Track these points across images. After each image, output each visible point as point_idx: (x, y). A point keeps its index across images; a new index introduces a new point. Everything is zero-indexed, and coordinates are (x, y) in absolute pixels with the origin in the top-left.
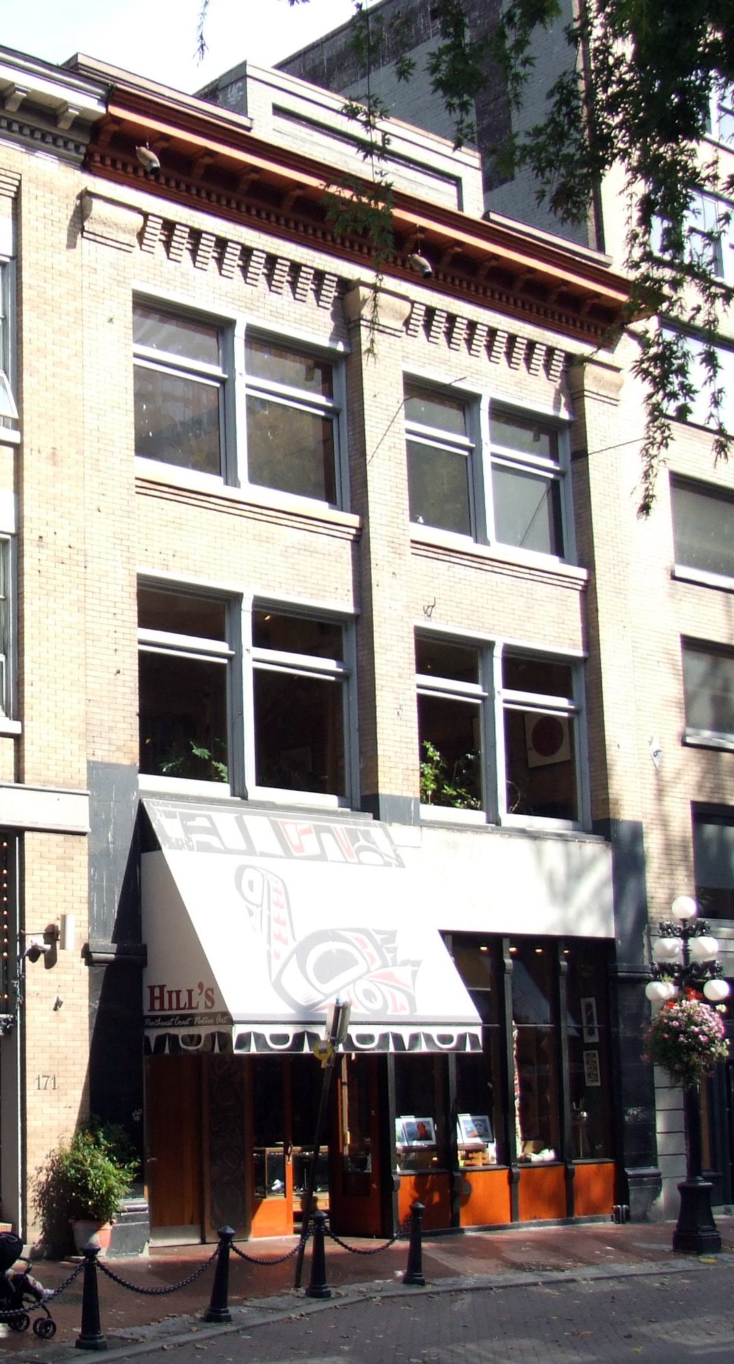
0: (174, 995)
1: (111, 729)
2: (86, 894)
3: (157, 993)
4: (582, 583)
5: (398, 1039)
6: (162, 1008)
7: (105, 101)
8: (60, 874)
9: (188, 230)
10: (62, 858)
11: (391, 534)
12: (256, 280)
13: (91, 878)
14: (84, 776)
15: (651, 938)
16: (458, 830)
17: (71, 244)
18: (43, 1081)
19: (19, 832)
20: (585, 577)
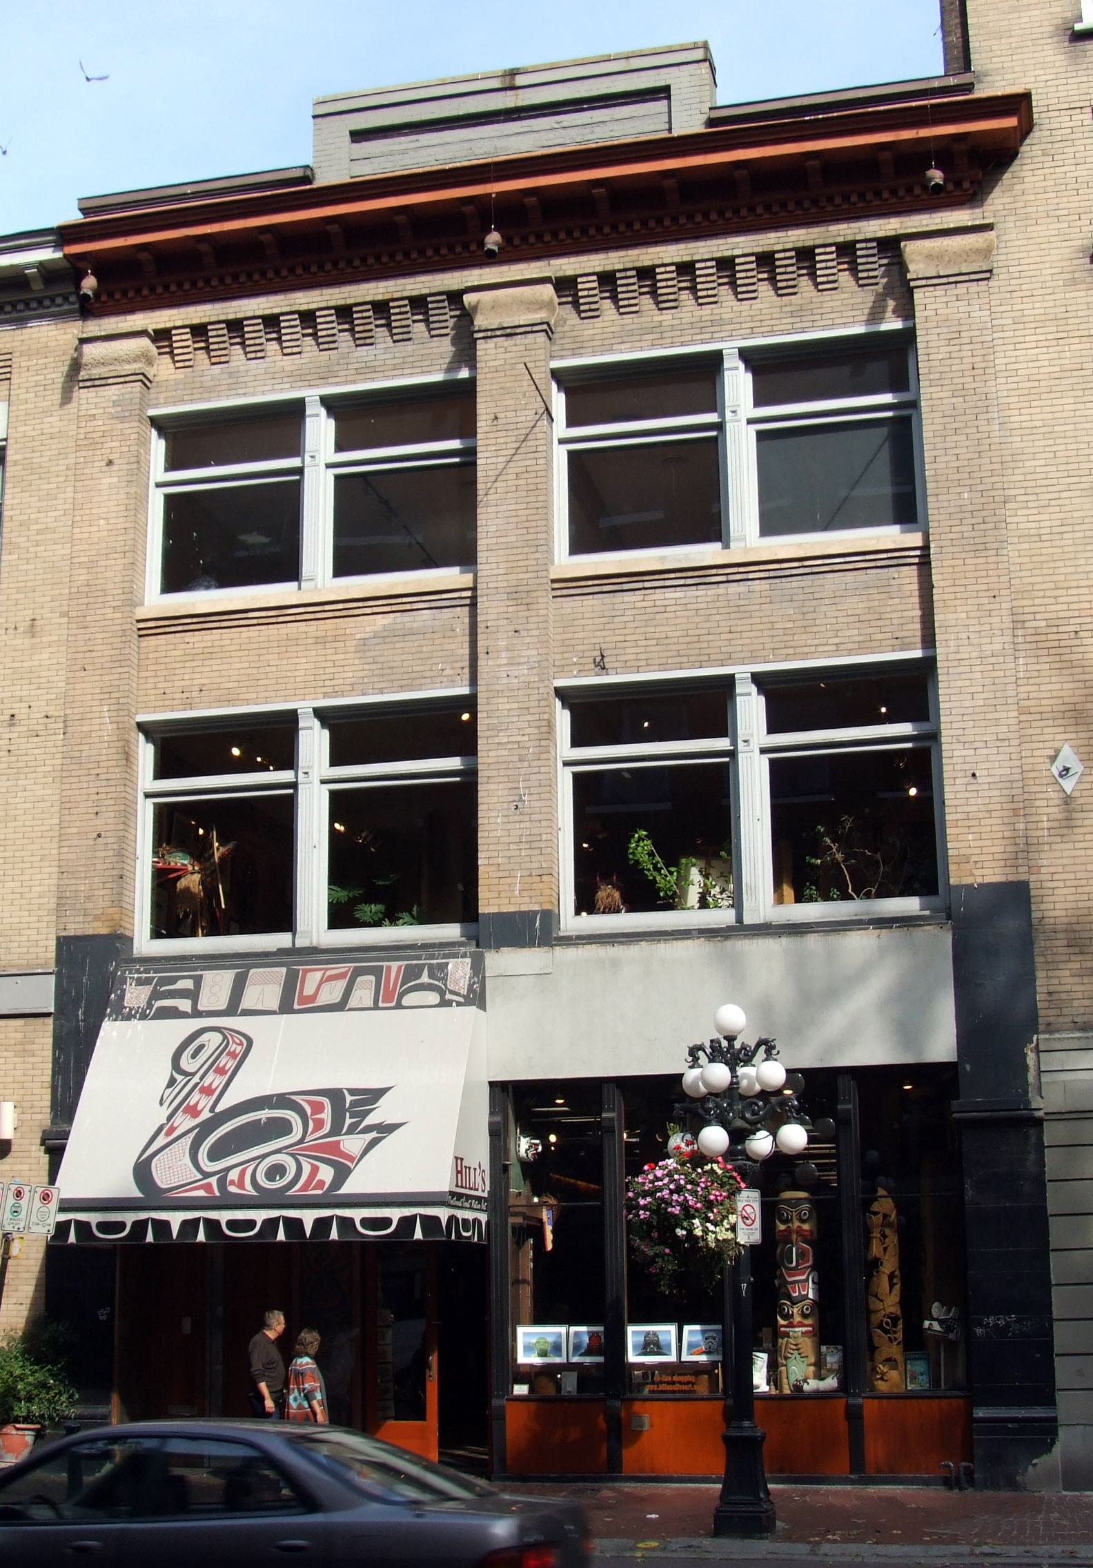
1: (88, 898)
2: (49, 1079)
4: (918, 553)
5: (294, 1226)
7: (58, 245)
8: (17, 1060)
9: (260, 321)
10: (21, 1044)
11: (514, 583)
12: (334, 342)
13: (55, 1061)
14: (52, 954)
15: (1041, 1054)
16: (621, 943)
17: (66, 398)
20: (919, 543)
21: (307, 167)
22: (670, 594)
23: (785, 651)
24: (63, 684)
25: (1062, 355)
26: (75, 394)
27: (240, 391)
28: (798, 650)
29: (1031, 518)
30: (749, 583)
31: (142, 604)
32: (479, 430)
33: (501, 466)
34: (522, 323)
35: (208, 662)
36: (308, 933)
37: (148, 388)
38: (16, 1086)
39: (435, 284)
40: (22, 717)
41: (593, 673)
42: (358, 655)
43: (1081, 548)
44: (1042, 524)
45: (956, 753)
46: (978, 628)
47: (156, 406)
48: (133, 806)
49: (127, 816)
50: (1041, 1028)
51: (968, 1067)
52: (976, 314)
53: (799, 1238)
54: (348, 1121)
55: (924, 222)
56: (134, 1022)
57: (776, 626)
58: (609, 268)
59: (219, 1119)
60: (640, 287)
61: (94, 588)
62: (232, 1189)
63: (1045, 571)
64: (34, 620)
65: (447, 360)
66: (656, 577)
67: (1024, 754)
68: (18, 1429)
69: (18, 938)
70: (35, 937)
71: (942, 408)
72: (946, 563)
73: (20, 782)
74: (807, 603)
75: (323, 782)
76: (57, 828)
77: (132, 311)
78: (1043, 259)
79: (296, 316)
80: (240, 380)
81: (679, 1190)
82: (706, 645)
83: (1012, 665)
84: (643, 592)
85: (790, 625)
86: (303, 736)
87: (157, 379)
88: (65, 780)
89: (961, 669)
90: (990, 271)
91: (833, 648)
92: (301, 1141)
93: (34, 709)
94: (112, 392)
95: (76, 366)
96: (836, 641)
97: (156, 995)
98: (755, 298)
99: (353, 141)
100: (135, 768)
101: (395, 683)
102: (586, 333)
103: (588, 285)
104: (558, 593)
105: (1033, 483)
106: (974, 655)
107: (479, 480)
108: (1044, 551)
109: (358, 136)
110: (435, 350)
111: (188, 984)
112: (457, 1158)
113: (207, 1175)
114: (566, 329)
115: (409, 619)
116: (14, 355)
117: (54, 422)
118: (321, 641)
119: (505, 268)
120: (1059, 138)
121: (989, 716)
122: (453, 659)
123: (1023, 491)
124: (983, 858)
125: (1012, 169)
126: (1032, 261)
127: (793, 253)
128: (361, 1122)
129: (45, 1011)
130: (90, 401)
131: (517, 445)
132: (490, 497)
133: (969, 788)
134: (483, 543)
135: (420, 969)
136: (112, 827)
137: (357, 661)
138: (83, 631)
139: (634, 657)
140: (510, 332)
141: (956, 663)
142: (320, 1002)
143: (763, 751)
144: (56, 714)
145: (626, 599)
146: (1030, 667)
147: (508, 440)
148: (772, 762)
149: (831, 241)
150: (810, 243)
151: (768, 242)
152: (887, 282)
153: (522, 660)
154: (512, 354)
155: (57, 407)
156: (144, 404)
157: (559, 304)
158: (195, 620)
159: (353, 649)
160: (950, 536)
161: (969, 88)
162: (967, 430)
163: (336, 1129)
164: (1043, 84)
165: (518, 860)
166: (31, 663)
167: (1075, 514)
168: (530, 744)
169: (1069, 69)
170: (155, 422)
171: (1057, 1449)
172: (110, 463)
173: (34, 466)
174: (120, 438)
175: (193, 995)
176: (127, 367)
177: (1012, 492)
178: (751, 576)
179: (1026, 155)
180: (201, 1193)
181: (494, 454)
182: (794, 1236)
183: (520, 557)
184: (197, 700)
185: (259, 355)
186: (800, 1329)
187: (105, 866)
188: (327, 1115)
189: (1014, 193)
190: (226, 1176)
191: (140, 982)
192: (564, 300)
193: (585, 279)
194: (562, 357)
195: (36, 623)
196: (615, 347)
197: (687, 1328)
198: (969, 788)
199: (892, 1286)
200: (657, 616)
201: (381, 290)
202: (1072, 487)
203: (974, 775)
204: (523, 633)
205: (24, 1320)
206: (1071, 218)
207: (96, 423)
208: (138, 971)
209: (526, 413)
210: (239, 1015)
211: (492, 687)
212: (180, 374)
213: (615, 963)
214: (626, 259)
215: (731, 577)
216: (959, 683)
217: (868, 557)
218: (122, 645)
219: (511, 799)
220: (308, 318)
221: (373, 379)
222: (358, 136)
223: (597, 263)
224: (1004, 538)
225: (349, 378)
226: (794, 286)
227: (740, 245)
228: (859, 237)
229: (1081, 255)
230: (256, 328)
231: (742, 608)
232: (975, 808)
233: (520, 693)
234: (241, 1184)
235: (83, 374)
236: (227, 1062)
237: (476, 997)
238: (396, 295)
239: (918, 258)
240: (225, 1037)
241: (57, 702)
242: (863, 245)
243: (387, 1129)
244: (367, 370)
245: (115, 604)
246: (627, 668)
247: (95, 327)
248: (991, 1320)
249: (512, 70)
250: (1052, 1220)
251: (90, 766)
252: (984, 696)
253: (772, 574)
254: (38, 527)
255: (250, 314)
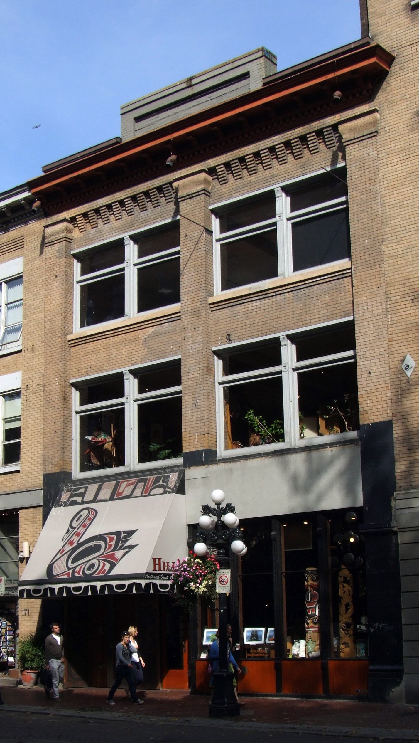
0: (166, 564)
1: (52, 457)
3: (157, 562)
5: (94, 588)
6: (160, 570)
11: (194, 307)
12: (133, 211)
16: (234, 461)
17: (41, 252)
18: (24, 612)
19: (17, 510)
21: (118, 137)
22: (255, 304)
23: (298, 324)
24: (43, 371)
25: (407, 166)
26: (44, 250)
27: (102, 238)
28: (304, 322)
29: (394, 248)
30: (285, 294)
31: (72, 333)
32: (181, 242)
33: (188, 257)
34: (195, 192)
35: (93, 355)
36: (129, 466)
37: (71, 242)
38: (31, 535)
39: (165, 180)
40: (31, 386)
41: (226, 343)
42: (144, 345)
43: (414, 259)
44: (399, 250)
45: (363, 363)
46: (371, 303)
47: (73, 250)
48: (214, 407)
49: (67, 422)
50: (397, 488)
51: (367, 509)
52: (371, 153)
53: (312, 589)
54: (120, 544)
55: (350, 114)
56: (62, 507)
57: (295, 313)
58: (227, 160)
59: (80, 545)
60: (242, 166)
61: (52, 329)
62: (76, 574)
63: (400, 272)
64: (33, 345)
65: (173, 212)
66: (248, 297)
67: (390, 360)
68: (28, 673)
69: (31, 476)
70: (36, 475)
71: (357, 201)
72: (358, 274)
73: (31, 413)
74: (307, 300)
75: (135, 401)
76: (42, 430)
77: (62, 211)
78: (399, 121)
79: (117, 203)
80: (102, 233)
81: (185, 570)
82: (268, 325)
83: (386, 319)
84: (245, 304)
85: (301, 311)
86: (126, 383)
87: (74, 238)
88: (45, 410)
89: (365, 323)
90: (377, 132)
91: (317, 320)
92: (102, 554)
93: (34, 382)
94: (56, 247)
95: (44, 238)
96: (318, 316)
97: (72, 496)
98: (286, 162)
99: (136, 122)
100: (70, 402)
101: (156, 356)
102: (223, 191)
103: (221, 169)
104: (213, 309)
105: (394, 231)
106: (370, 316)
107: (181, 264)
108: (399, 263)
109: (138, 119)
110: (168, 209)
111: (82, 491)
112: (154, 559)
113: (69, 569)
114: (215, 190)
115: (161, 328)
116: (25, 236)
117: (38, 262)
118: (131, 341)
119: (189, 168)
120: (407, 60)
121: (376, 344)
122: (176, 343)
123: (390, 235)
124: (373, 411)
125: (386, 80)
126: (394, 123)
127: (298, 139)
128: (124, 545)
129: (39, 505)
130: (49, 251)
131: (194, 247)
132: (185, 271)
133: (368, 379)
134: (183, 291)
135: (160, 478)
136: (59, 428)
137: (143, 349)
138: (49, 348)
139: (241, 334)
140: (191, 196)
141: (362, 321)
142: (124, 495)
143: (294, 370)
144: (41, 383)
145: (238, 308)
146: (393, 319)
147: (191, 244)
148: (298, 374)
149: (312, 130)
150: (304, 133)
151: (287, 136)
152: (339, 145)
153: (196, 341)
154: (193, 206)
155: (38, 256)
156: (68, 249)
157: (213, 179)
158: (87, 338)
159: (141, 344)
160: (360, 261)
161: (368, 43)
162: (367, 210)
163: (115, 549)
164: (399, 35)
165: (196, 428)
166: (33, 363)
167: (412, 243)
168: (200, 377)
169: (411, 24)
170: (75, 256)
171: (403, 685)
172: (56, 276)
173: (32, 282)
174: (59, 266)
175: (83, 495)
176: (60, 235)
177: (386, 236)
178: (285, 291)
179: (392, 72)
180: (66, 577)
181: (186, 251)
182: (309, 588)
183: (195, 296)
184: (90, 371)
185: (108, 221)
186: (312, 629)
187: (58, 444)
188: (113, 543)
189: (387, 91)
190: (75, 569)
191: (68, 491)
192: (214, 177)
193: (219, 167)
194: (214, 203)
195: (34, 347)
196: (233, 195)
197: (269, 629)
198: (368, 379)
199: (347, 610)
200: (250, 315)
201: (146, 186)
202: (411, 230)
203: (370, 373)
204: (197, 329)
205: (35, 630)
206: (411, 98)
207: (51, 261)
208: (68, 487)
209: (197, 231)
210: (97, 502)
211: (187, 354)
212: (81, 235)
213: (231, 470)
214: (234, 155)
215: (277, 293)
216: (364, 330)
217: (330, 276)
218: (61, 352)
219: (193, 402)
220: (121, 203)
221: (147, 225)
222: (138, 119)
223: (230, 156)
224: (382, 259)
225: (139, 226)
226: (301, 154)
227: (276, 140)
228: (323, 126)
229: (416, 116)
230: (104, 211)
231: (282, 306)
232: (370, 388)
233: (196, 355)
234: (79, 573)
235: (46, 241)
236: (87, 522)
237: (181, 489)
238: (151, 188)
239: (346, 132)
240: (89, 512)
241: (41, 378)
242: (326, 130)
243: (131, 547)
244: (145, 222)
245: (59, 335)
246: (239, 340)
247: (50, 220)
248: (377, 625)
249: (191, 78)
250: (402, 578)
251: (52, 403)
252: (374, 335)
253: (293, 289)
254: (34, 307)
255: (101, 205)
